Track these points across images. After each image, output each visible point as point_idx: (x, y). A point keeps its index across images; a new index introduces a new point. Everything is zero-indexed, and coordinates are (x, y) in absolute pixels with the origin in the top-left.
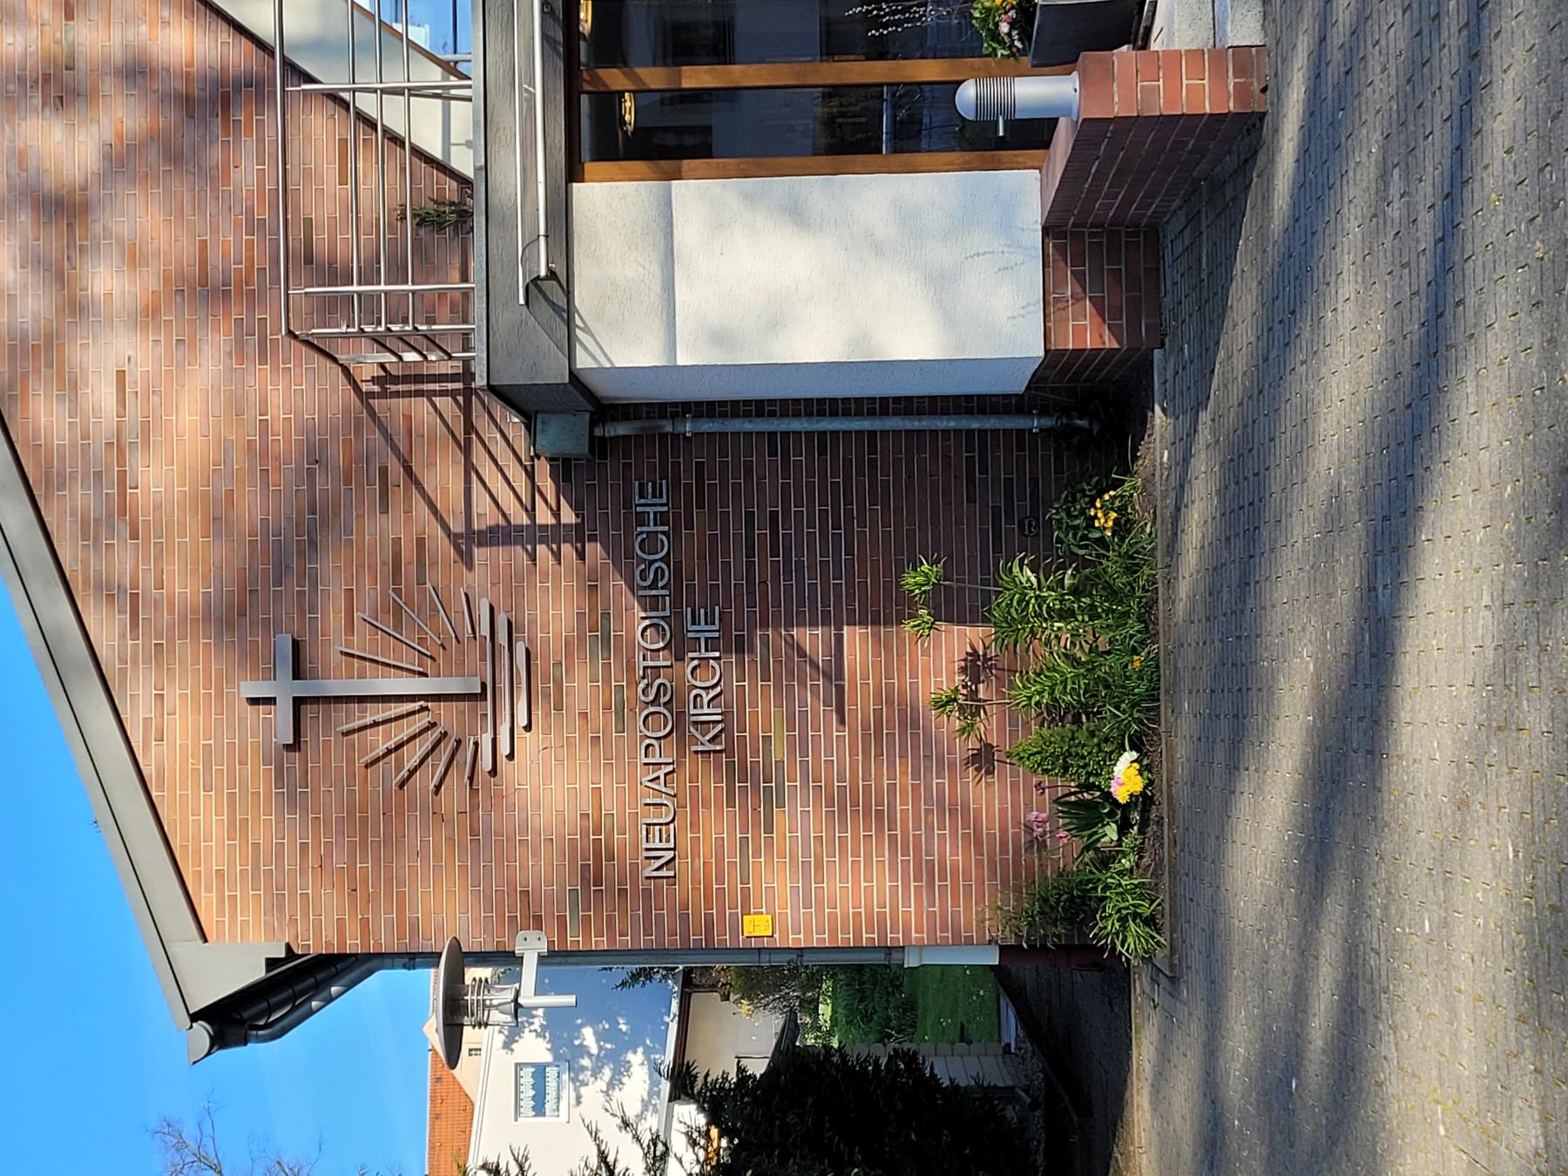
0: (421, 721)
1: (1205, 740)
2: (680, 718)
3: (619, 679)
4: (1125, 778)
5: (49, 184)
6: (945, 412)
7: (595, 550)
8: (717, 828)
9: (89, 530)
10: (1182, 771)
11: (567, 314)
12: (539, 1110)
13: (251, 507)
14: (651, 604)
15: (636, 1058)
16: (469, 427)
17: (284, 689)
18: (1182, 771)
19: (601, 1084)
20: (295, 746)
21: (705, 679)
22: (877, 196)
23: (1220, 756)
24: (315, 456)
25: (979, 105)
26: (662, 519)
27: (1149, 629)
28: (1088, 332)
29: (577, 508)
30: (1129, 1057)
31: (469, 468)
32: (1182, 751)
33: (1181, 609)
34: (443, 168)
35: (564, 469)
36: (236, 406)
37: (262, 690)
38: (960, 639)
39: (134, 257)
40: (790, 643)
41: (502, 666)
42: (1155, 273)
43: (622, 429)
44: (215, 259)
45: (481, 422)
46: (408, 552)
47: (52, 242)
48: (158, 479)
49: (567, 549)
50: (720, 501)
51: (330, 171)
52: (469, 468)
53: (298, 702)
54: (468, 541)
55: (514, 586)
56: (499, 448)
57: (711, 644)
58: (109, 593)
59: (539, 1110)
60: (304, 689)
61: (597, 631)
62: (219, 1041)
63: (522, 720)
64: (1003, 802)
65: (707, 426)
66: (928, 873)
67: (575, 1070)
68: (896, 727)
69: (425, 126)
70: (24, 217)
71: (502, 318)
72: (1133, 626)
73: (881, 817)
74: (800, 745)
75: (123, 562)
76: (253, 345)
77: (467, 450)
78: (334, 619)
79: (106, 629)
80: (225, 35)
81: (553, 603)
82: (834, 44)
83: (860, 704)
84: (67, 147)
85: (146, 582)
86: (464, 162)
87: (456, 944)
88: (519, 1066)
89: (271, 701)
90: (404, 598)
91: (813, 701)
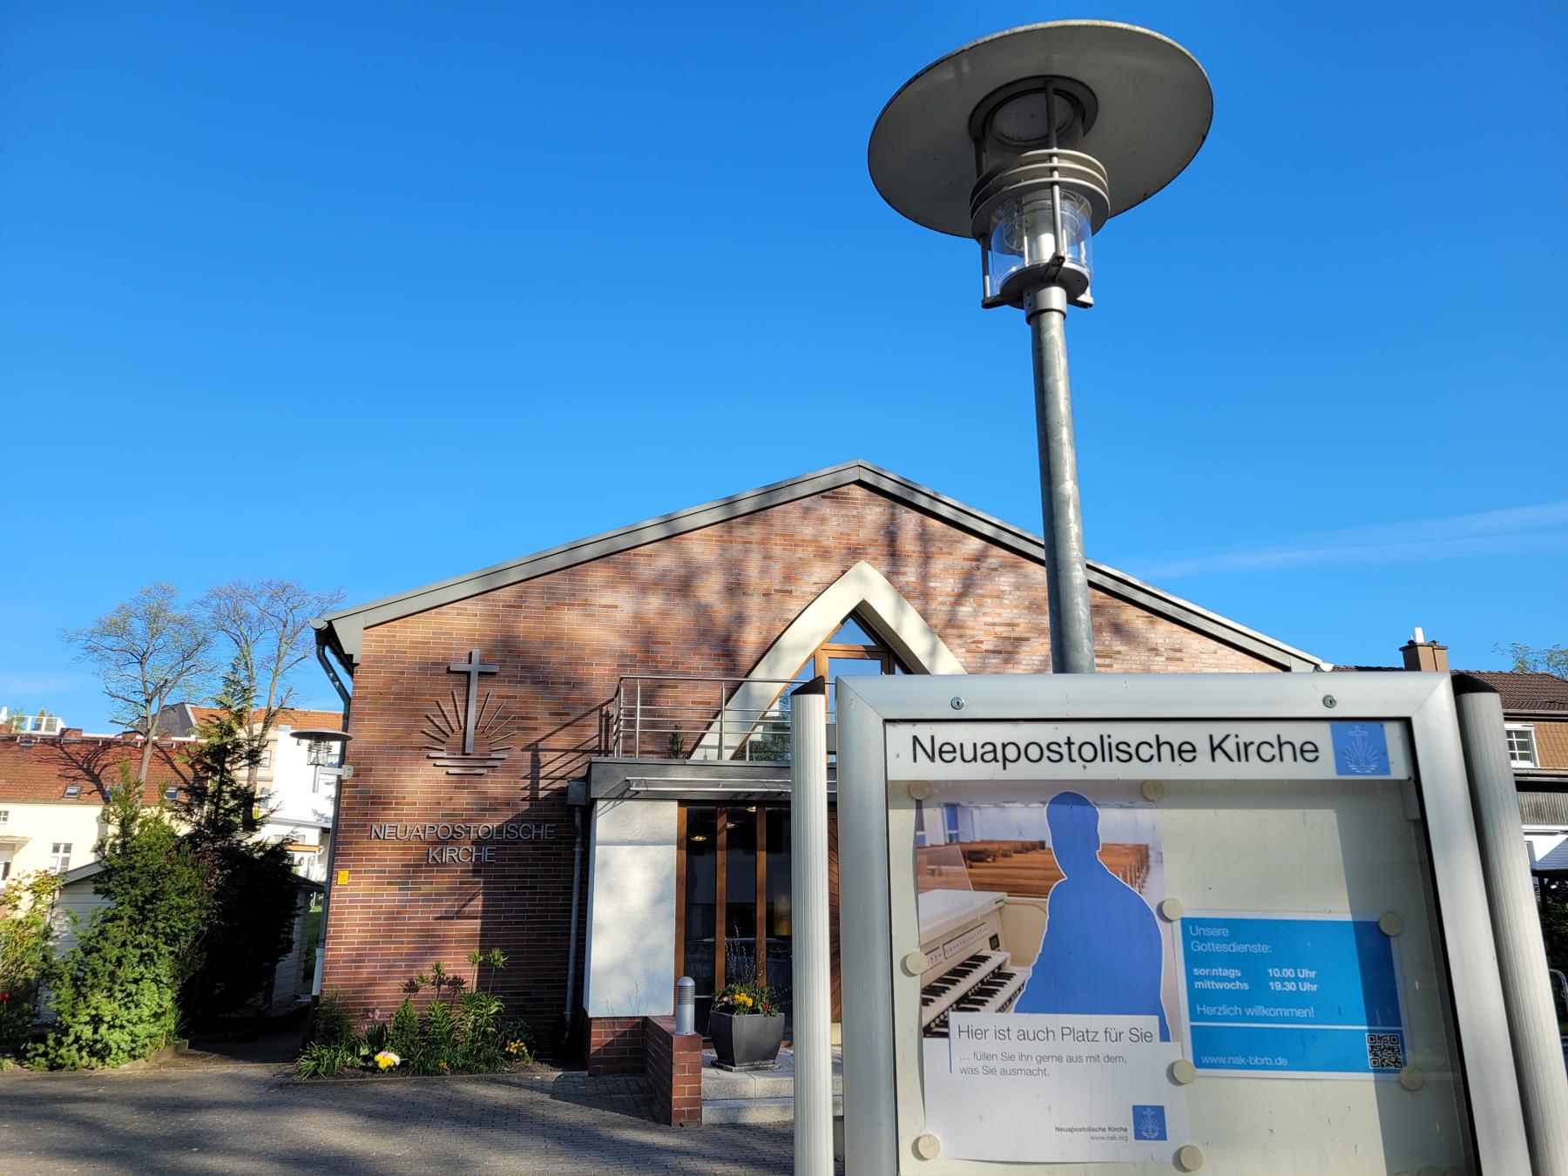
0: (455, 726)
1: (397, 1101)
4: (388, 1058)
5: (697, 582)
6: (576, 969)
8: (391, 858)
10: (383, 1088)
13: (555, 657)
14: (499, 830)
16: (584, 752)
17: (474, 668)
18: (383, 1088)
20: (449, 671)
21: (461, 854)
22: (665, 937)
23: (380, 1108)
24: (575, 684)
27: (456, 1070)
28: (599, 1038)
29: (546, 798)
31: (567, 751)
32: (392, 1088)
33: (462, 1087)
34: (696, 745)
35: (562, 792)
36: (600, 653)
37: (475, 658)
38: (470, 976)
39: (664, 614)
41: (474, 760)
43: (578, 820)
44: (661, 648)
46: (531, 723)
48: (570, 621)
51: (698, 697)
52: (567, 751)
53: (468, 673)
54: (534, 749)
55: (511, 769)
56: (574, 765)
57: (478, 858)
58: (521, 596)
60: (474, 677)
61: (490, 806)
62: (319, 632)
63: (451, 771)
64: (388, 996)
65: (577, 858)
66: (359, 959)
68: (430, 943)
69: (710, 739)
70: (683, 572)
71: (617, 769)
75: (534, 602)
76: (624, 661)
77: (574, 751)
78: (505, 691)
80: (755, 657)
85: (524, 612)
86: (698, 755)
87: (350, 738)
90: (508, 720)
91: (447, 905)
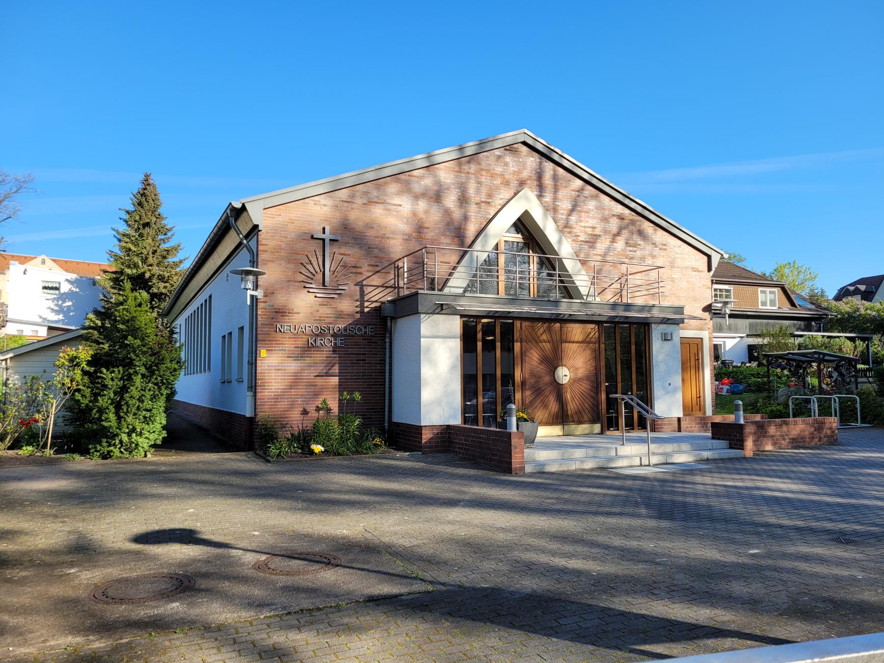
2: (317, 335)
3: (328, 320)
7: (358, 316)
8: (289, 344)
9: (366, 193)
11: (433, 313)
12: (45, 288)
13: (371, 233)
15: (61, 317)
16: (387, 287)
17: (327, 236)
19: (53, 306)
20: (312, 237)
21: (328, 343)
25: (511, 409)
26: (365, 333)
28: (426, 436)
29: (368, 312)
30: (213, 452)
31: (378, 287)
35: (377, 310)
36: (394, 233)
39: (426, 212)
40: (335, 364)
42: (438, 452)
44: (426, 230)
45: (389, 290)
46: (359, 270)
47: (431, 193)
48: (377, 211)
49: (359, 309)
50: (370, 348)
52: (378, 287)
53: (324, 240)
54: (361, 285)
58: (353, 196)
59: (45, 288)
60: (327, 241)
61: (340, 315)
63: (318, 295)
66: (277, 398)
67: (57, 299)
72: (354, 449)
73: (291, 387)
74: (310, 366)
75: (359, 201)
76: (408, 239)
77: (382, 286)
79: (343, 194)
80: (472, 239)
81: (348, 306)
82: (484, 376)
83: (320, 381)
84: (451, 201)
85: (354, 206)
88: (60, 283)
89: (324, 233)
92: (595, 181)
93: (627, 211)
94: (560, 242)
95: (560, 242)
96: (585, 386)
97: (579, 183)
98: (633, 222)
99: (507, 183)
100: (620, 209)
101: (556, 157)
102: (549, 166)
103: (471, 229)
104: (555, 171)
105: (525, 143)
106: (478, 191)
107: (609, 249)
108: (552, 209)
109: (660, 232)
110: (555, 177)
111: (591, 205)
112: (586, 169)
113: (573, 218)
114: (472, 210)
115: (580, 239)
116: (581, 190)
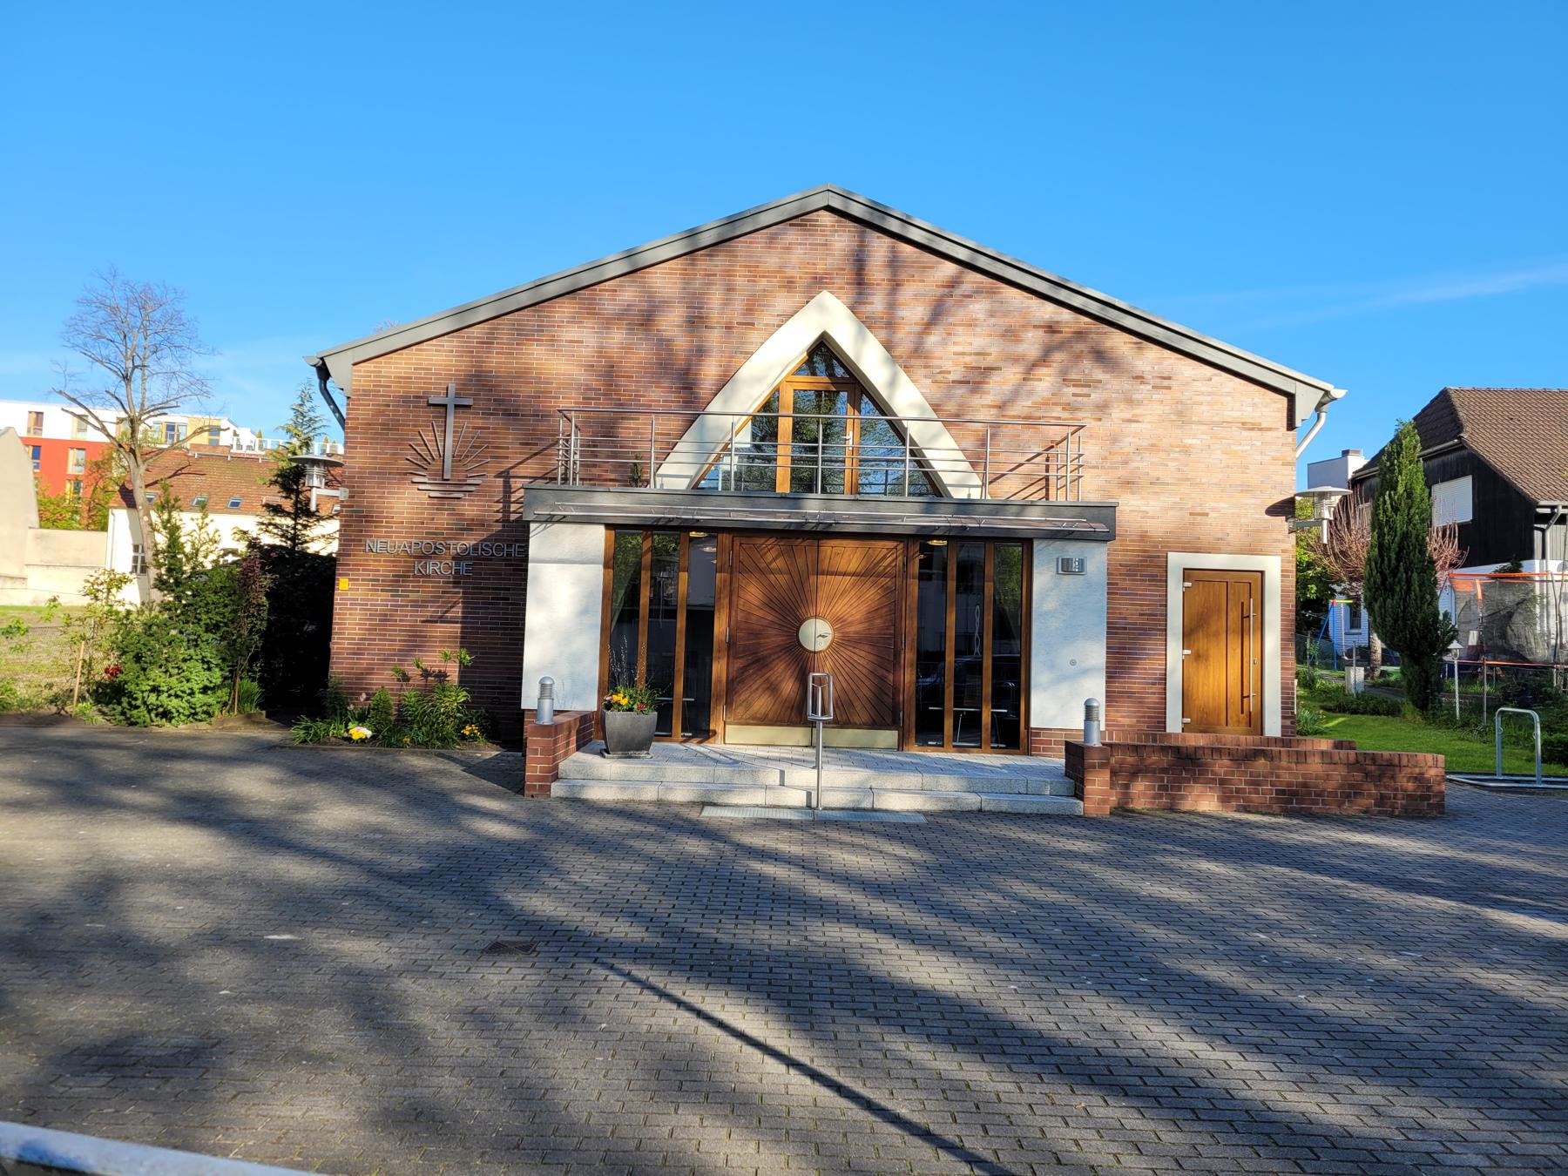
21: (440, 567)
26: (509, 554)
54: (506, 476)
61: (469, 526)
66: (358, 652)
76: (588, 393)
84: (671, 322)
92: (982, 262)
93: (1066, 315)
94: (893, 383)
95: (893, 383)
96: (862, 658)
97: (950, 269)
98: (1080, 335)
99: (789, 285)
100: (1048, 311)
101: (894, 226)
102: (880, 246)
103: (710, 370)
104: (893, 251)
105: (829, 208)
106: (727, 303)
107: (1016, 394)
108: (885, 326)
109: (1154, 352)
110: (894, 263)
111: (978, 308)
112: (963, 237)
113: (932, 339)
114: (714, 337)
115: (951, 377)
116: (953, 283)
